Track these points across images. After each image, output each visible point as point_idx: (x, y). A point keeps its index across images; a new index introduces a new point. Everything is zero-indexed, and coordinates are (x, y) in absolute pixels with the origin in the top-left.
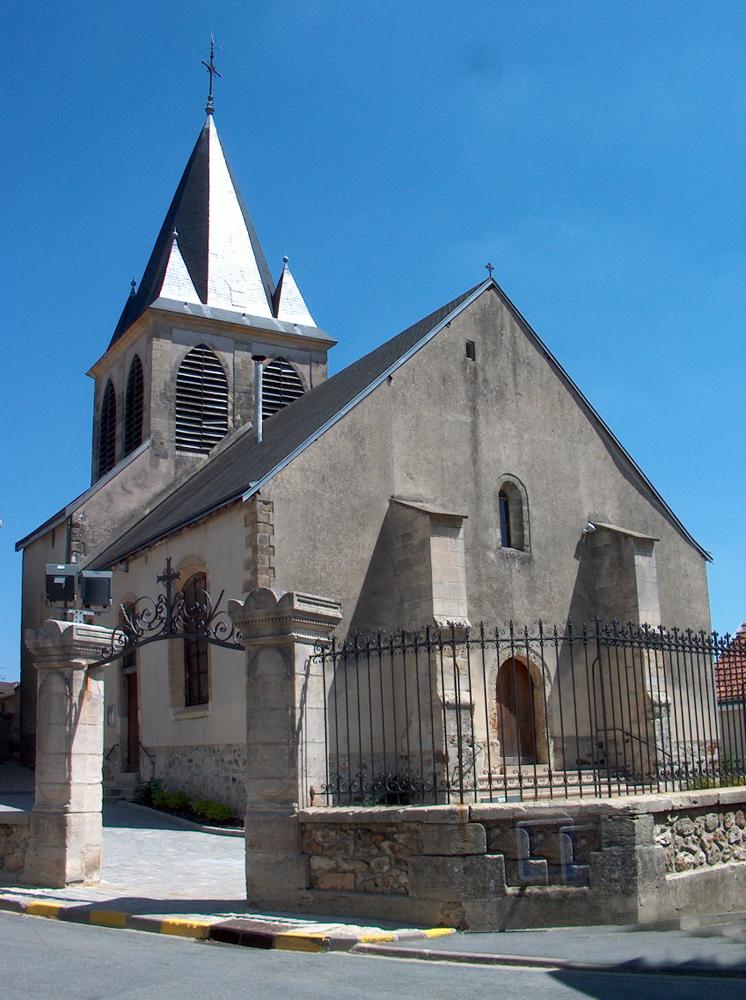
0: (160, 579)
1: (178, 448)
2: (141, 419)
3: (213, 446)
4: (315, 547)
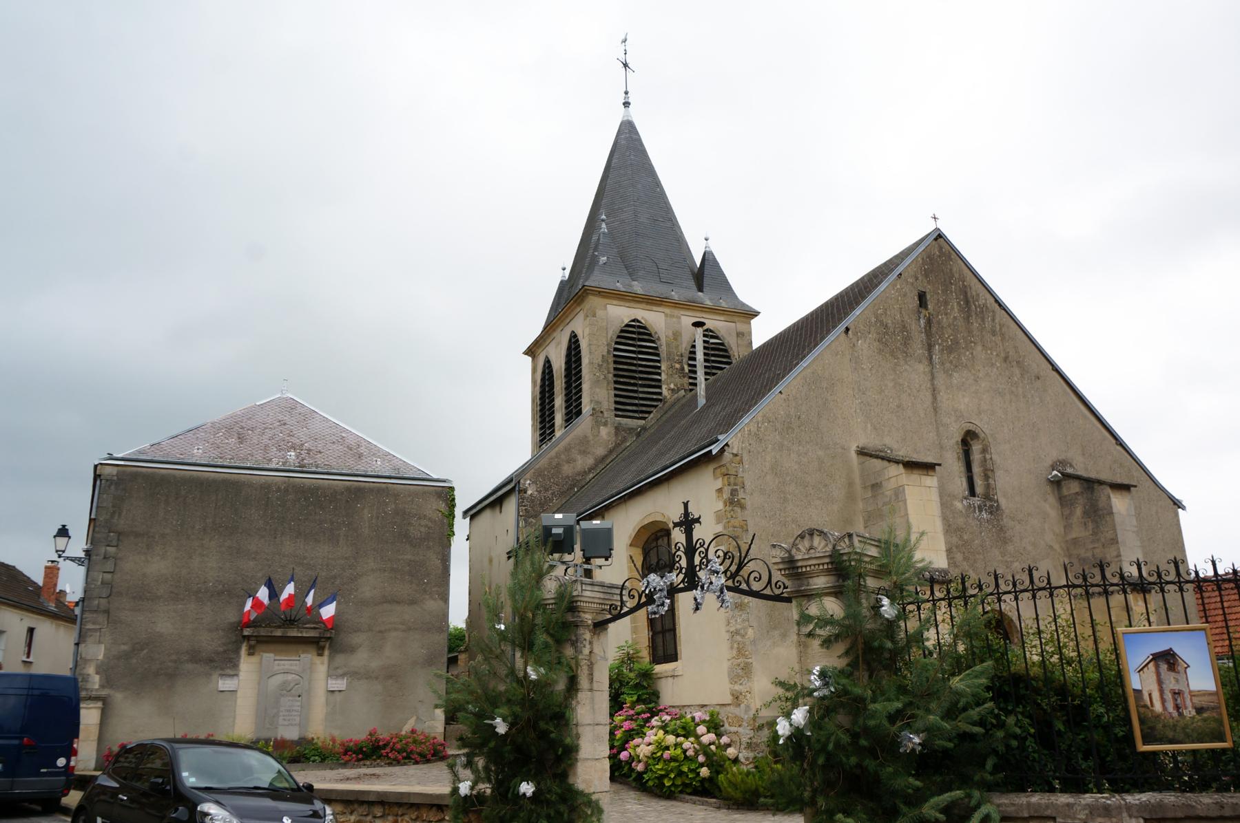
0: (698, 520)
1: (617, 416)
2: (580, 390)
3: (650, 413)
4: (785, 500)
